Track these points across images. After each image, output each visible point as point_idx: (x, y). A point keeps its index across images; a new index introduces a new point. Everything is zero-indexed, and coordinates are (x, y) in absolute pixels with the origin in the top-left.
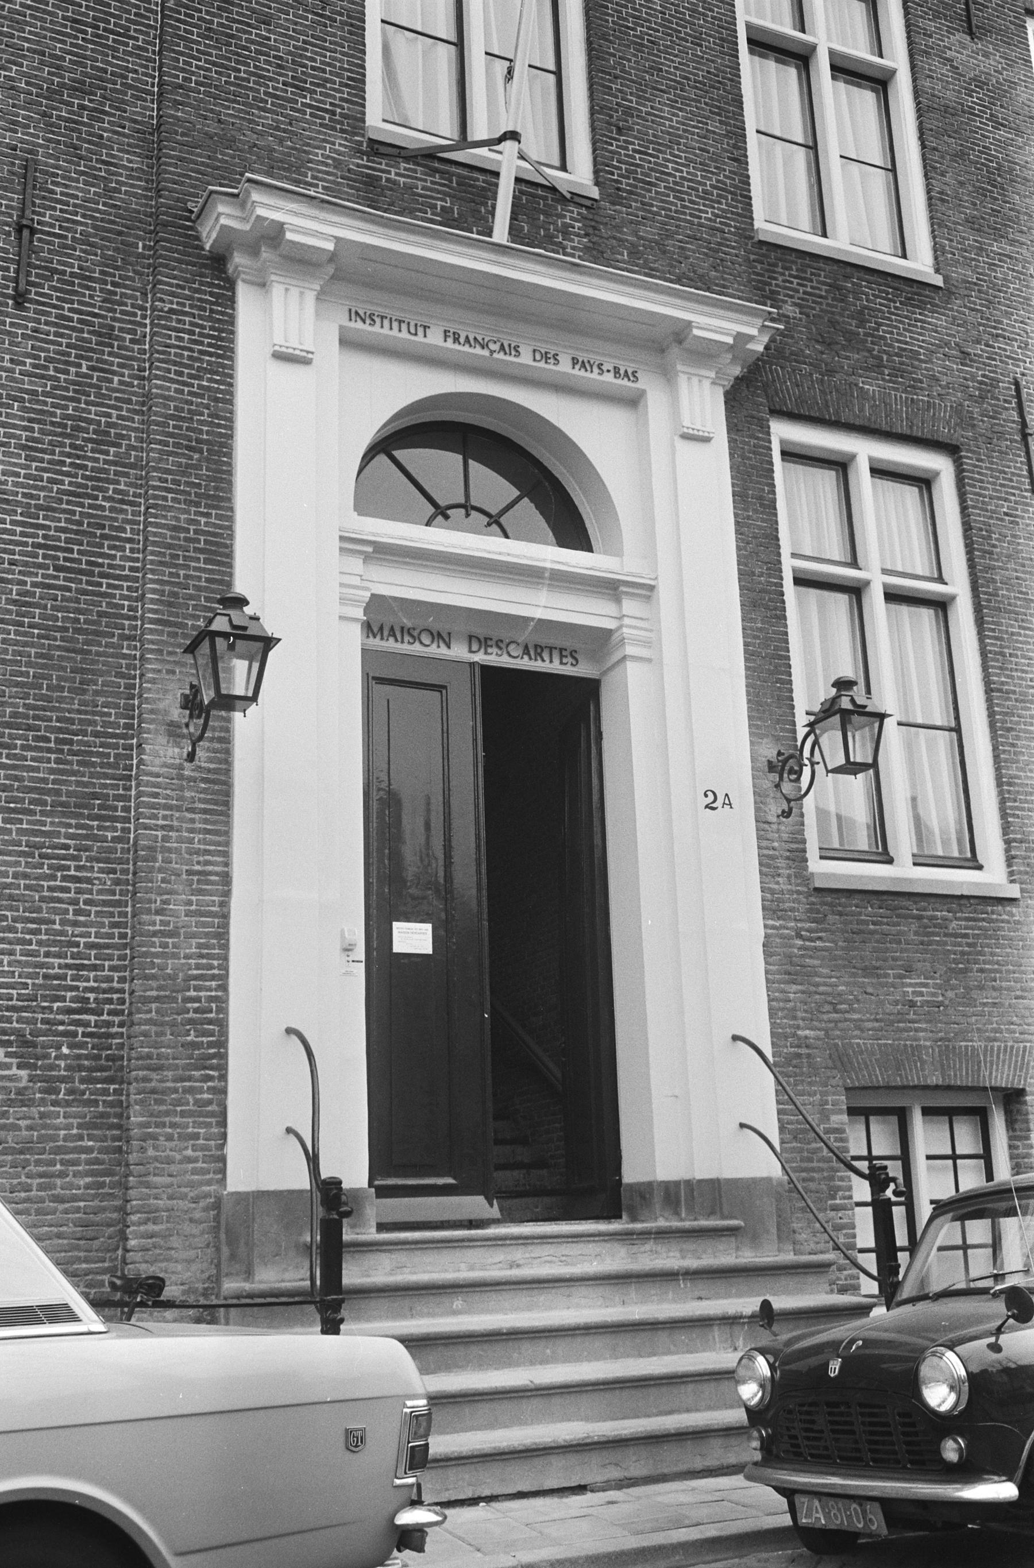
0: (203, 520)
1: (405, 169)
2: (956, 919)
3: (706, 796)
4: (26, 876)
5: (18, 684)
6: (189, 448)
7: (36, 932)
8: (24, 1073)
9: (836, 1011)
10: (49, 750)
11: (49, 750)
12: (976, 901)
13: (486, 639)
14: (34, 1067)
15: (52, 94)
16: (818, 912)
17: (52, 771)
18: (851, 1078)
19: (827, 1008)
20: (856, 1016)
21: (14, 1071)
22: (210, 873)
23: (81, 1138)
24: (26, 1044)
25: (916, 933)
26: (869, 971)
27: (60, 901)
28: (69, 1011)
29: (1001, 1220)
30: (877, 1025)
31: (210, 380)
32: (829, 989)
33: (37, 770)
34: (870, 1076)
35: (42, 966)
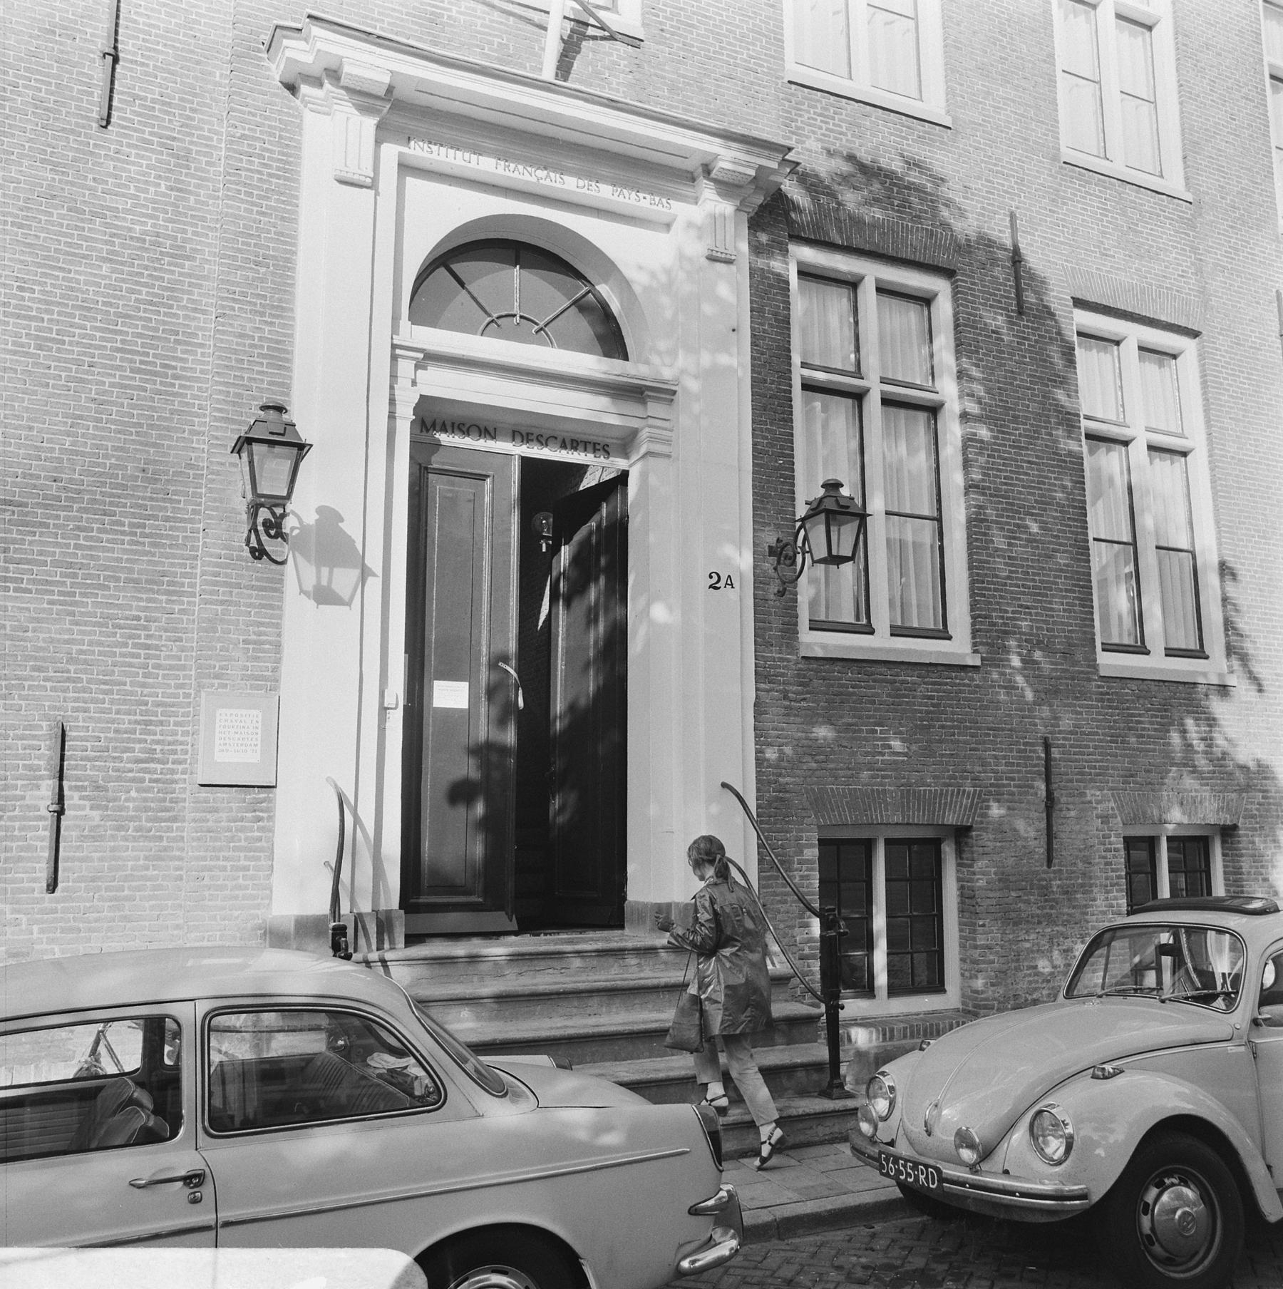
0: (267, 328)
4: (100, 644)
10: (123, 533)
11: (123, 533)
17: (125, 551)
18: (823, 817)
20: (832, 766)
21: (87, 812)
22: (263, 643)
24: (97, 788)
25: (889, 695)
27: (131, 665)
28: (138, 761)
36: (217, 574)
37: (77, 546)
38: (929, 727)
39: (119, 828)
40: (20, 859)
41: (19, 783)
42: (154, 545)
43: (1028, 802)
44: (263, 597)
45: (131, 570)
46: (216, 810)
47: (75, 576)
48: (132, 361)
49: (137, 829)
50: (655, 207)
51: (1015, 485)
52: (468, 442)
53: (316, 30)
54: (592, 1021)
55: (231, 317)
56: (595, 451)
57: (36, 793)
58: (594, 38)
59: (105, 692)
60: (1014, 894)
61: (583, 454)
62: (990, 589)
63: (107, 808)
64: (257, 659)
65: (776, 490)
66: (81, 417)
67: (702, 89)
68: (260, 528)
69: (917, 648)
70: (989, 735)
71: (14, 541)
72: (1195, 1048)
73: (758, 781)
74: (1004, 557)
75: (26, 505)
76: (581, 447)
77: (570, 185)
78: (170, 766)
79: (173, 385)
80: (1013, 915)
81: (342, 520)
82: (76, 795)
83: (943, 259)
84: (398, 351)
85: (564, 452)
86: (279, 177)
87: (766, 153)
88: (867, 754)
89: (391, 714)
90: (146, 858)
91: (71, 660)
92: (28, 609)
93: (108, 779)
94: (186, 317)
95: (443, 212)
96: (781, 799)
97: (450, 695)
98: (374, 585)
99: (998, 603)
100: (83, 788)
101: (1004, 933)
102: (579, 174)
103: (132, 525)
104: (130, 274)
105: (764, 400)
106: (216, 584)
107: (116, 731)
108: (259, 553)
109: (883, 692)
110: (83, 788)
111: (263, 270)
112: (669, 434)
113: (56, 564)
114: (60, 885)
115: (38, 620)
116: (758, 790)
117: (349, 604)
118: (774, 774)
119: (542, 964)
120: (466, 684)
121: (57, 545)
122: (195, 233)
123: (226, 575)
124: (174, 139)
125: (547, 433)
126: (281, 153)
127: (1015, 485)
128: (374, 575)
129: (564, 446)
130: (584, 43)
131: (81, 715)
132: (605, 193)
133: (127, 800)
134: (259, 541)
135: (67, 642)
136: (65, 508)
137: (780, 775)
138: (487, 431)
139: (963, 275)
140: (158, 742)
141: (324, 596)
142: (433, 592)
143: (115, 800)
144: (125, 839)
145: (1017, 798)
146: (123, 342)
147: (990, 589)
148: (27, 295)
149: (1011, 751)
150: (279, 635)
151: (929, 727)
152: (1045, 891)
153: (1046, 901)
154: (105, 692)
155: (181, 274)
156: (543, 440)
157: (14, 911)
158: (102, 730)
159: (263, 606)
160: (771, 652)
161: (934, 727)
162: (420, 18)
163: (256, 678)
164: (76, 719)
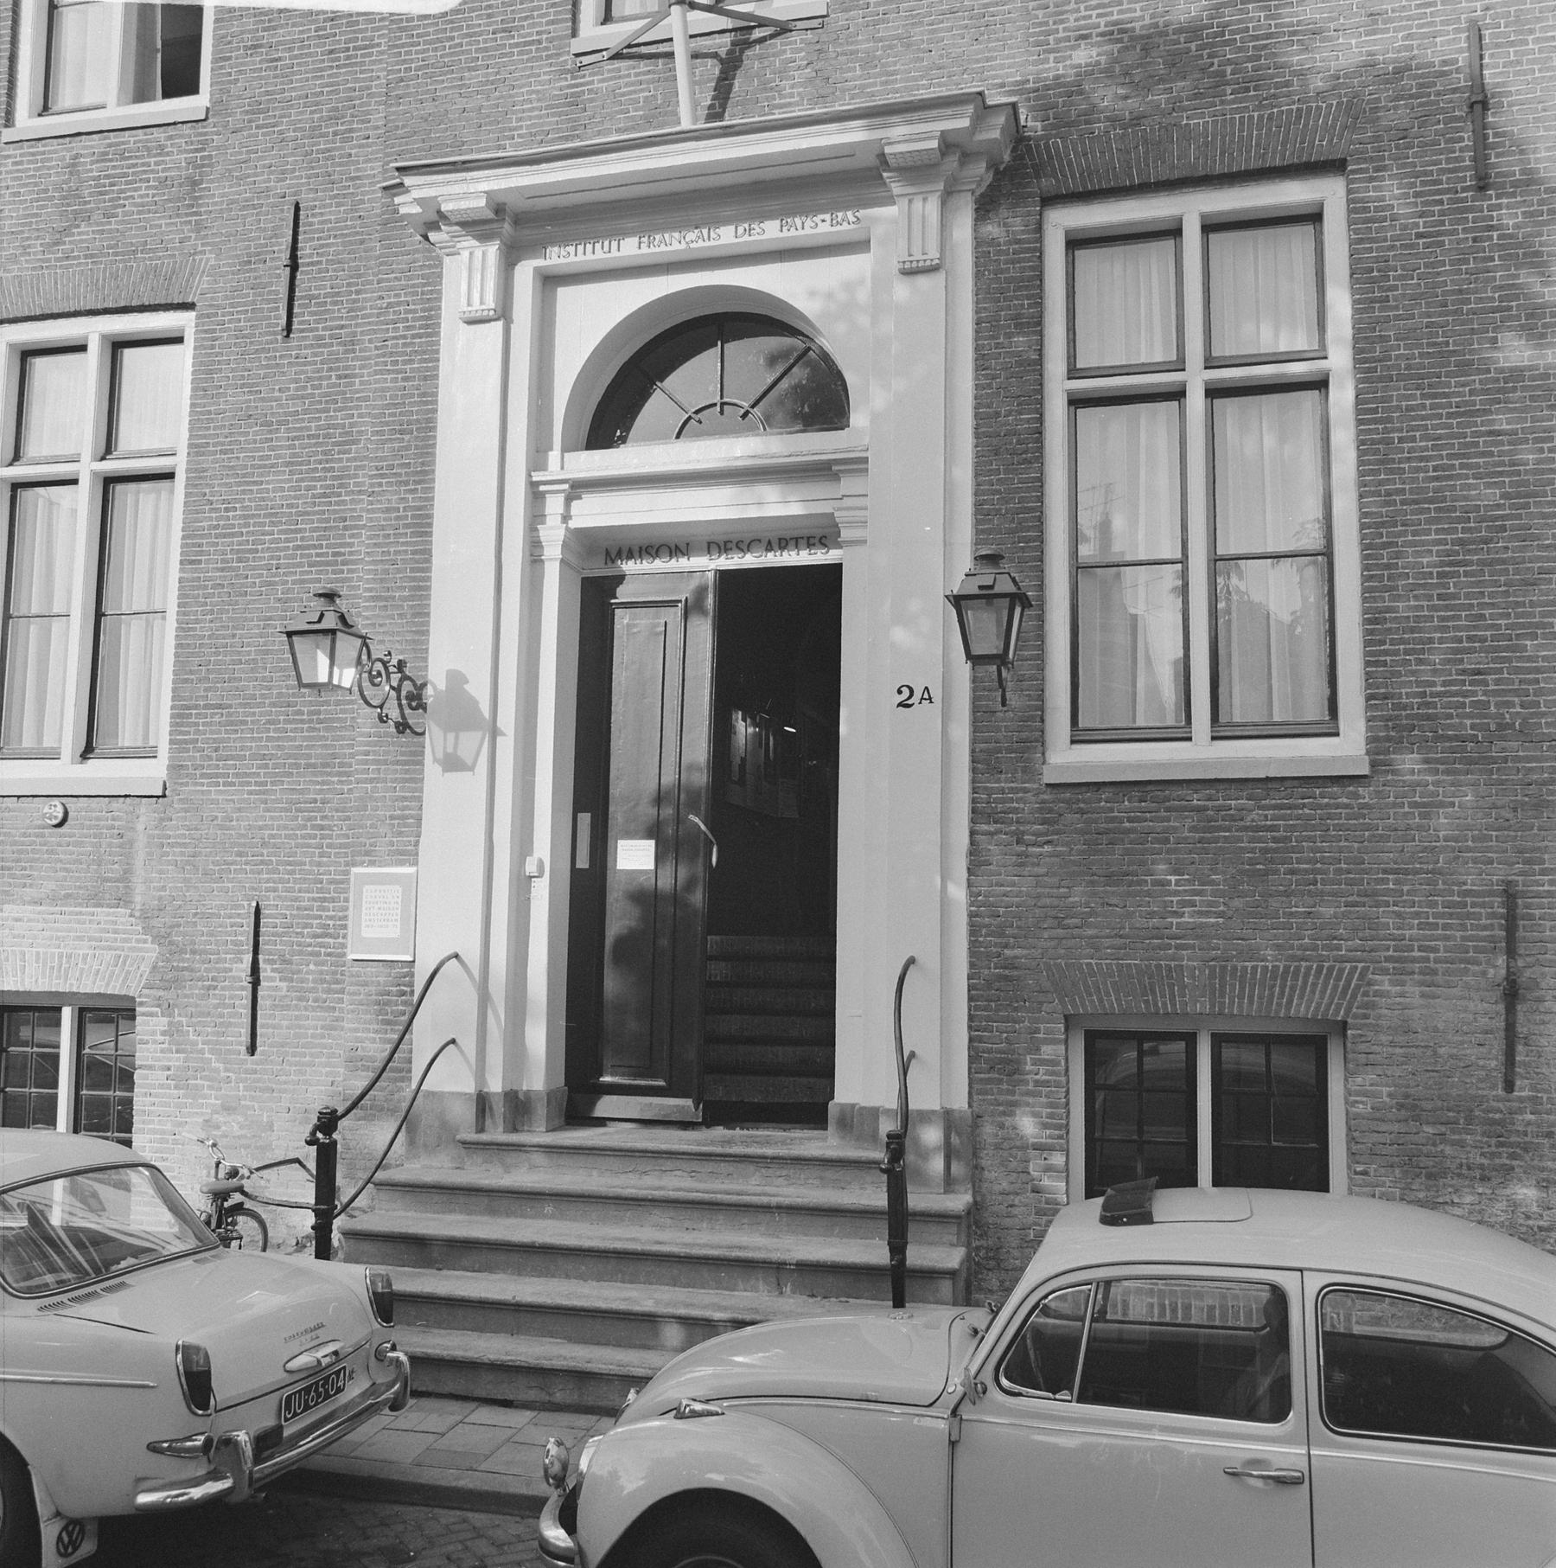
0: (410, 497)
2: (1259, 808)
3: (900, 692)
4: (285, 828)
6: (401, 432)
7: (292, 872)
8: (284, 985)
9: (1060, 926)
10: (302, 721)
11: (302, 721)
12: (1296, 783)
14: (292, 980)
15: (315, 132)
16: (1050, 811)
17: (305, 739)
19: (1049, 922)
20: (1090, 932)
22: (407, 817)
23: (323, 1037)
24: (285, 961)
25: (1193, 829)
27: (309, 846)
28: (316, 936)
30: (1118, 941)
31: (421, 361)
33: (294, 739)
34: (1101, 1001)
37: (269, 739)
38: (1266, 873)
42: (327, 729)
44: (407, 772)
45: (309, 756)
47: (266, 767)
48: (310, 556)
49: (316, 1000)
50: (839, 228)
53: (408, 181)
55: (379, 493)
58: (762, 40)
59: (290, 873)
60: (1429, 1129)
64: (400, 834)
66: (270, 619)
68: (404, 702)
69: (1258, 754)
71: (223, 740)
72: (864, 1405)
73: (972, 953)
75: (230, 706)
77: (726, 237)
80: (1424, 1162)
82: (269, 967)
83: (1322, 147)
84: (542, 488)
87: (949, 111)
88: (1151, 915)
89: (535, 883)
91: (264, 845)
93: (293, 953)
94: (352, 501)
95: (594, 318)
96: (1006, 978)
99: (1413, 673)
100: (274, 962)
101: (1408, 1188)
103: (311, 713)
105: (995, 441)
106: (366, 762)
109: (1183, 826)
110: (274, 962)
111: (407, 437)
112: (862, 513)
113: (254, 757)
114: (259, 1049)
115: (240, 810)
116: (972, 965)
117: (471, 769)
118: (996, 945)
119: (669, 1164)
120: (652, 843)
123: (375, 753)
125: (748, 537)
126: (424, 310)
129: (769, 547)
130: (748, 53)
132: (771, 231)
135: (261, 828)
136: (259, 705)
139: (1358, 161)
140: (331, 918)
141: (452, 764)
143: (299, 972)
144: (306, 1009)
145: (1439, 979)
146: (302, 539)
147: (1396, 653)
150: (420, 808)
151: (1266, 873)
154: (290, 873)
156: (743, 546)
157: (226, 1070)
158: (287, 908)
159: (407, 781)
160: (998, 781)
161: (1276, 872)
164: (268, 899)
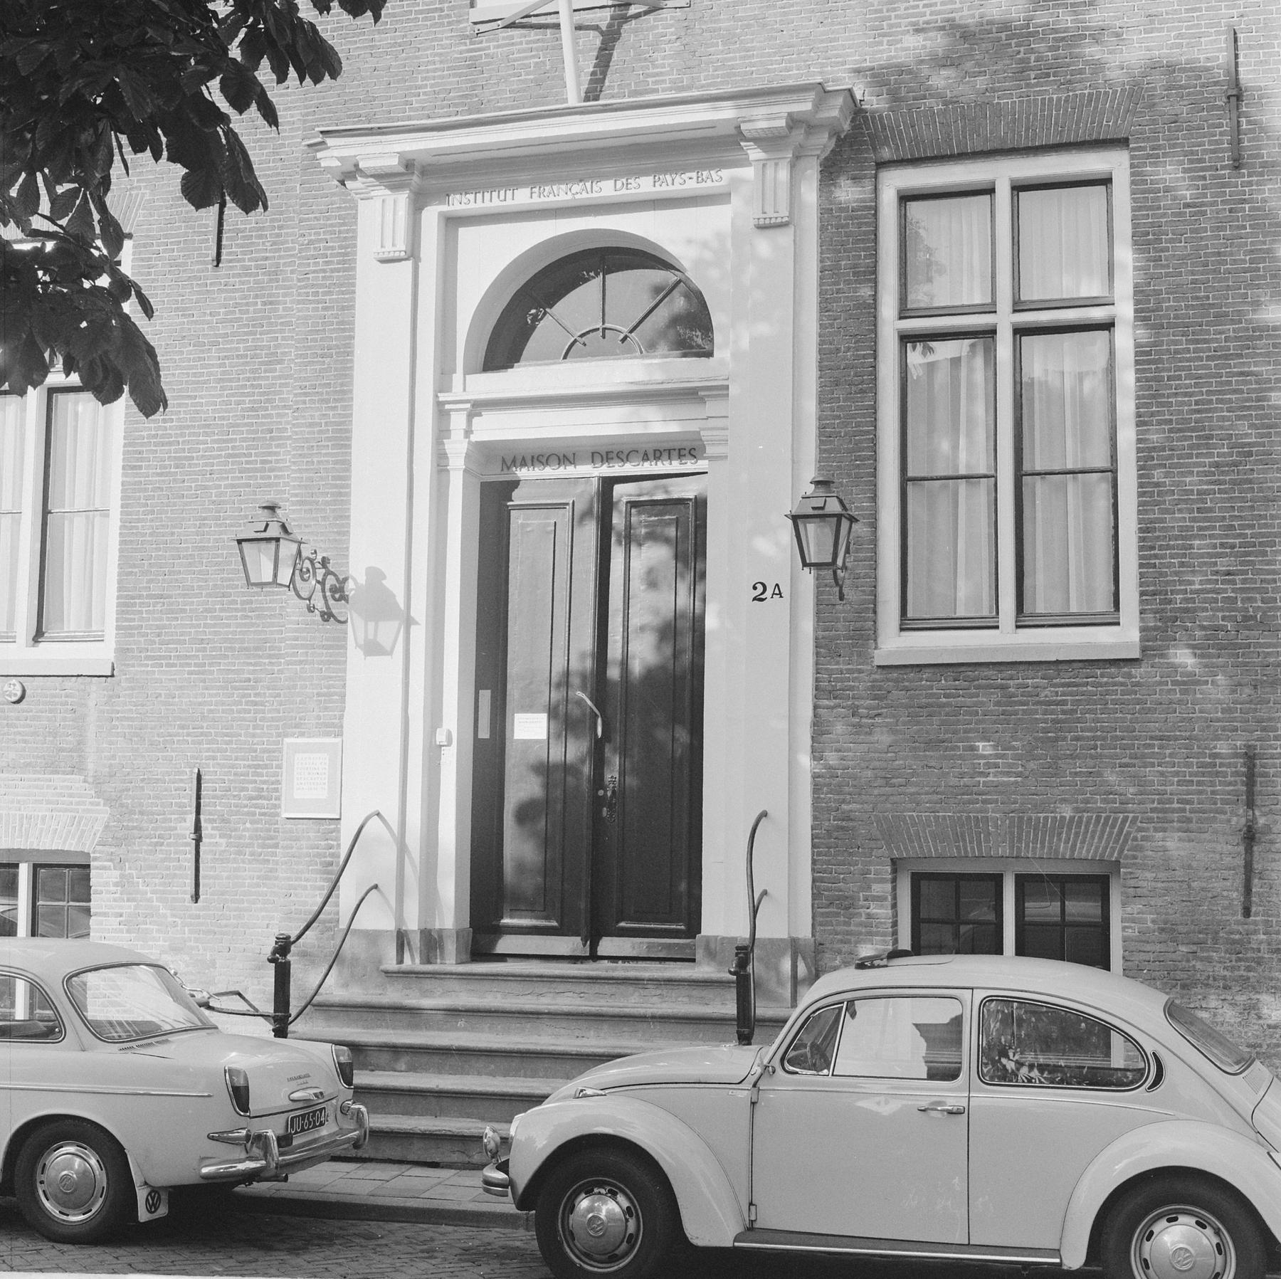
1: (504, 38)
3: (755, 588)
5: (217, 564)
8: (223, 841)
9: (887, 784)
10: (236, 610)
11: (236, 610)
13: (607, 453)
17: (238, 625)
18: (898, 849)
19: (880, 782)
20: (912, 790)
21: (217, 840)
25: (998, 704)
26: (932, 744)
27: (244, 719)
28: (251, 798)
29: (735, 991)
30: (936, 797)
32: (884, 764)
34: (921, 847)
35: (233, 766)
36: (296, 639)
38: (1056, 740)
39: (239, 853)
40: (175, 876)
41: (173, 817)
42: (258, 617)
43: (1215, 832)
45: (243, 641)
46: (297, 839)
47: (204, 650)
50: (703, 185)
51: (1216, 410)
52: (549, 472)
53: (330, 141)
54: (579, 1042)
56: (680, 456)
57: (183, 824)
58: (637, 16)
60: (1184, 949)
61: (667, 463)
62: (1163, 557)
63: (230, 837)
64: (326, 709)
65: (849, 475)
66: (205, 519)
67: (764, 25)
68: (328, 594)
70: (1152, 746)
71: (164, 627)
74: (1191, 511)
76: (665, 455)
77: (606, 189)
78: (273, 802)
79: (270, 477)
80: (1179, 975)
81: (385, 578)
82: (210, 826)
85: (647, 464)
86: (338, 270)
90: (259, 878)
92: (175, 680)
94: (279, 415)
95: (493, 255)
97: (530, 727)
98: (419, 635)
99: (1176, 574)
100: (214, 821)
102: (615, 176)
103: (243, 603)
104: (238, 387)
105: (836, 373)
107: (235, 774)
108: (327, 616)
110: (214, 821)
112: (723, 433)
114: (202, 897)
116: (815, 818)
117: (390, 653)
121: (192, 626)
122: (284, 338)
124: (267, 258)
127: (1216, 410)
128: (417, 623)
129: (646, 458)
130: (625, 26)
131: (211, 762)
132: (645, 186)
133: (244, 830)
134: (327, 606)
135: (200, 704)
136: (196, 596)
137: (844, 801)
138: (565, 458)
140: (264, 782)
141: (373, 648)
142: (910, 539)
143: (236, 830)
148: (168, 425)
149: (1189, 765)
151: (1056, 740)
152: (1238, 948)
153: (1239, 960)
155: (274, 378)
159: (331, 663)
160: (838, 663)
162: (459, 68)
163: (327, 725)
